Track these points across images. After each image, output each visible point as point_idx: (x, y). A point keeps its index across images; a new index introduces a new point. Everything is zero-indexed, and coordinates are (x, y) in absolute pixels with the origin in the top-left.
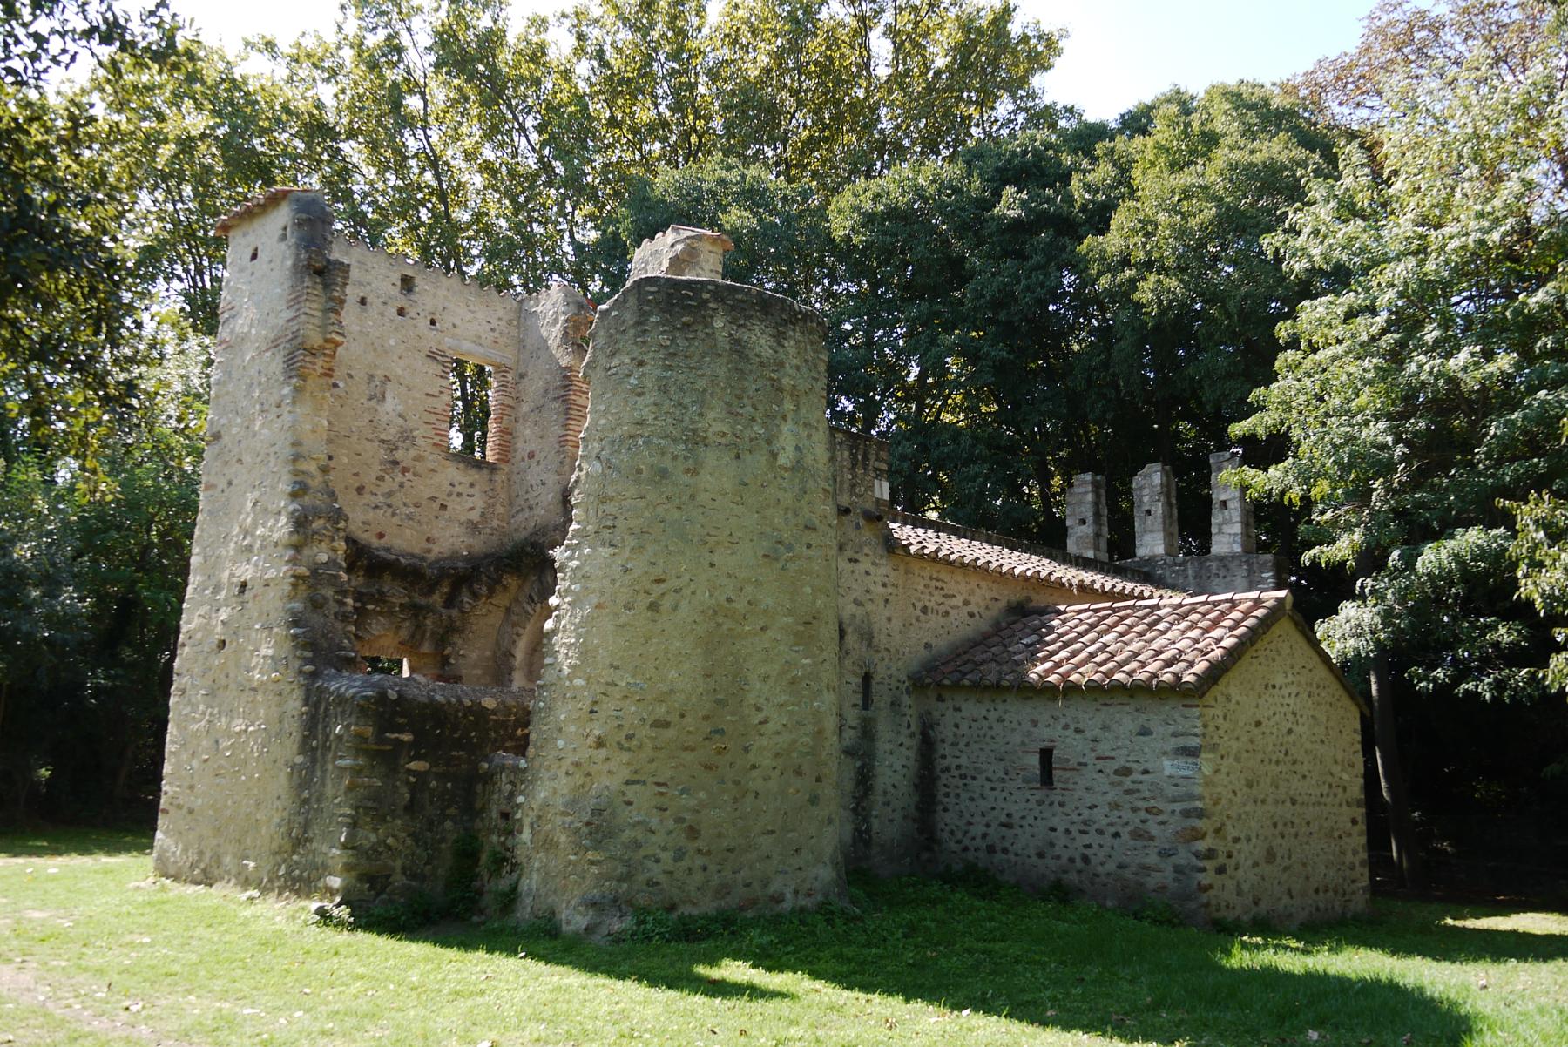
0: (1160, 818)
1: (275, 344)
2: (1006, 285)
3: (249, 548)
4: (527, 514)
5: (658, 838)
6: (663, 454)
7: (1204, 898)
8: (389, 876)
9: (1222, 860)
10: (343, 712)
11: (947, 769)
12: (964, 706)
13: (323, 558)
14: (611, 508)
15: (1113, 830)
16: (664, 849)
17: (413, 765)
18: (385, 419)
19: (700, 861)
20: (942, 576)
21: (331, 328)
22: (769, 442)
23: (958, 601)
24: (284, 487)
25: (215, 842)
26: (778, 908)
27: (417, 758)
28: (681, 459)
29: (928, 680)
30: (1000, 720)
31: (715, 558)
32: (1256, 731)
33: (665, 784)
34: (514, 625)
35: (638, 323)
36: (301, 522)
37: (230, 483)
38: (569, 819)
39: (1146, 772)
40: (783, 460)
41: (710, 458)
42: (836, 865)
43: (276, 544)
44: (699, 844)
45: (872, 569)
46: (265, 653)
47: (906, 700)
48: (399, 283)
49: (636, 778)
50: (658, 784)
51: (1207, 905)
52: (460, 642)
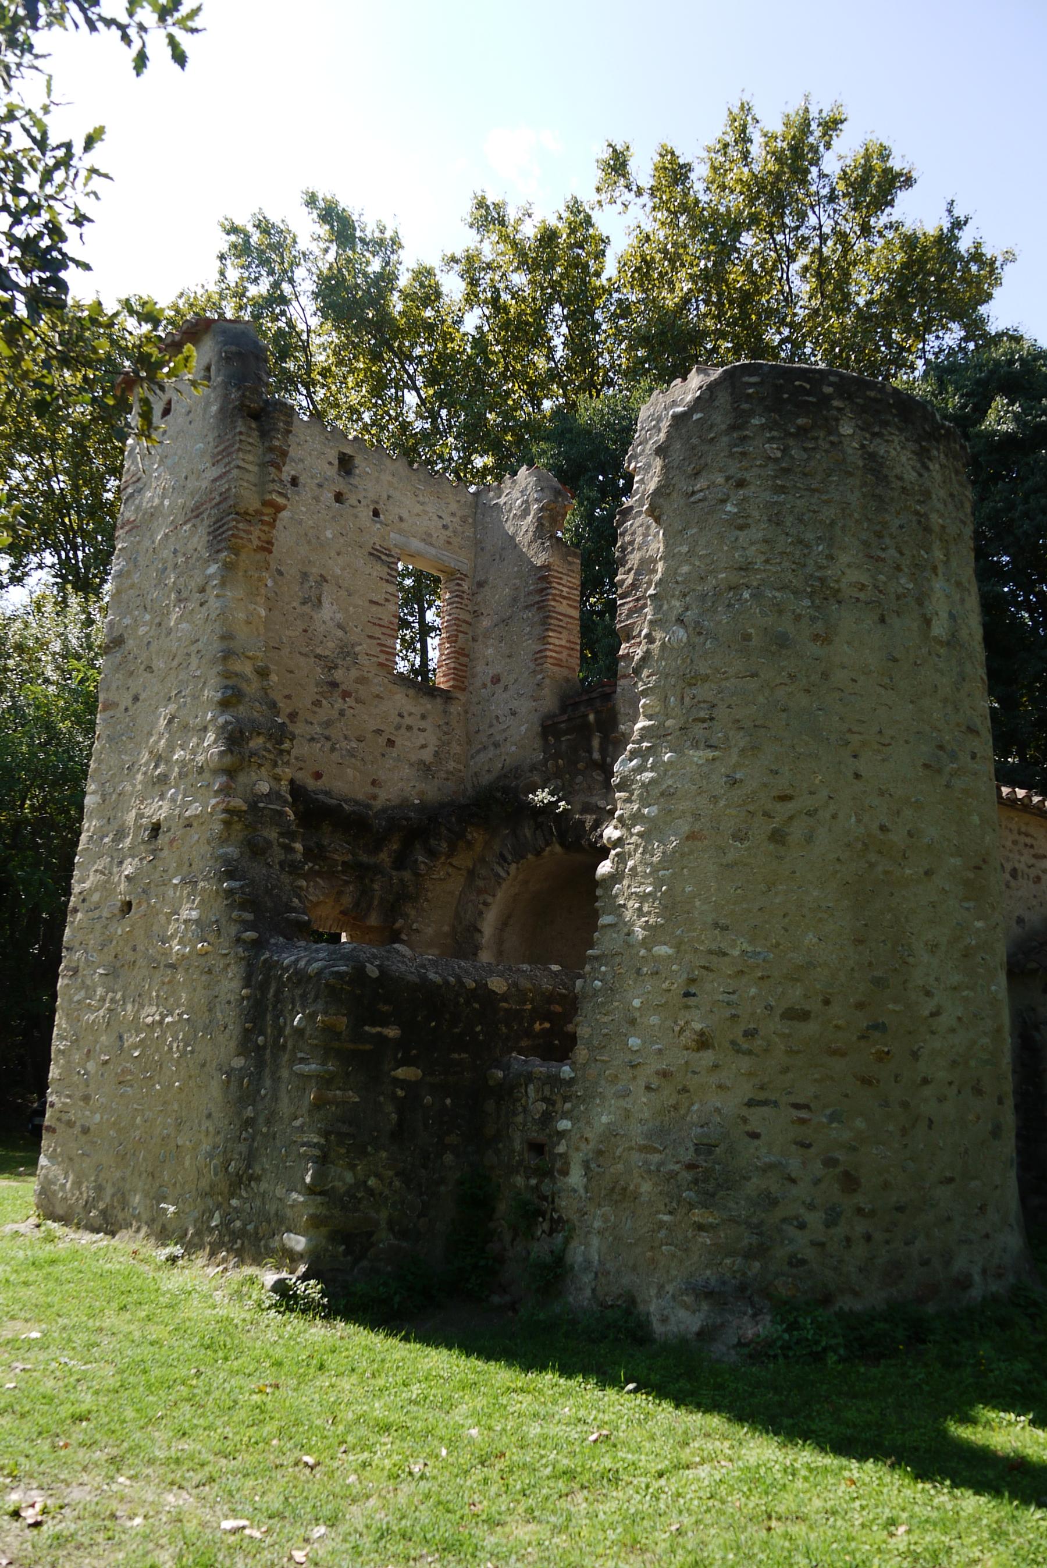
1: (196, 513)
3: (163, 779)
4: (491, 752)
6: (780, 612)
8: (371, 1234)
10: (304, 996)
13: (264, 787)
14: (705, 691)
16: (811, 1207)
17: (401, 1073)
18: (322, 629)
19: (861, 1227)
20: (1032, 830)
21: (271, 486)
22: (920, 603)
24: (211, 693)
25: (118, 1174)
29: (1032, 965)
33: (806, 1107)
34: (480, 892)
35: (733, 428)
36: (234, 739)
37: (136, 699)
38: (656, 1158)
40: (939, 628)
43: (201, 770)
44: (860, 1199)
46: (185, 916)
48: (336, 462)
49: (762, 1096)
50: (796, 1106)
52: (413, 913)
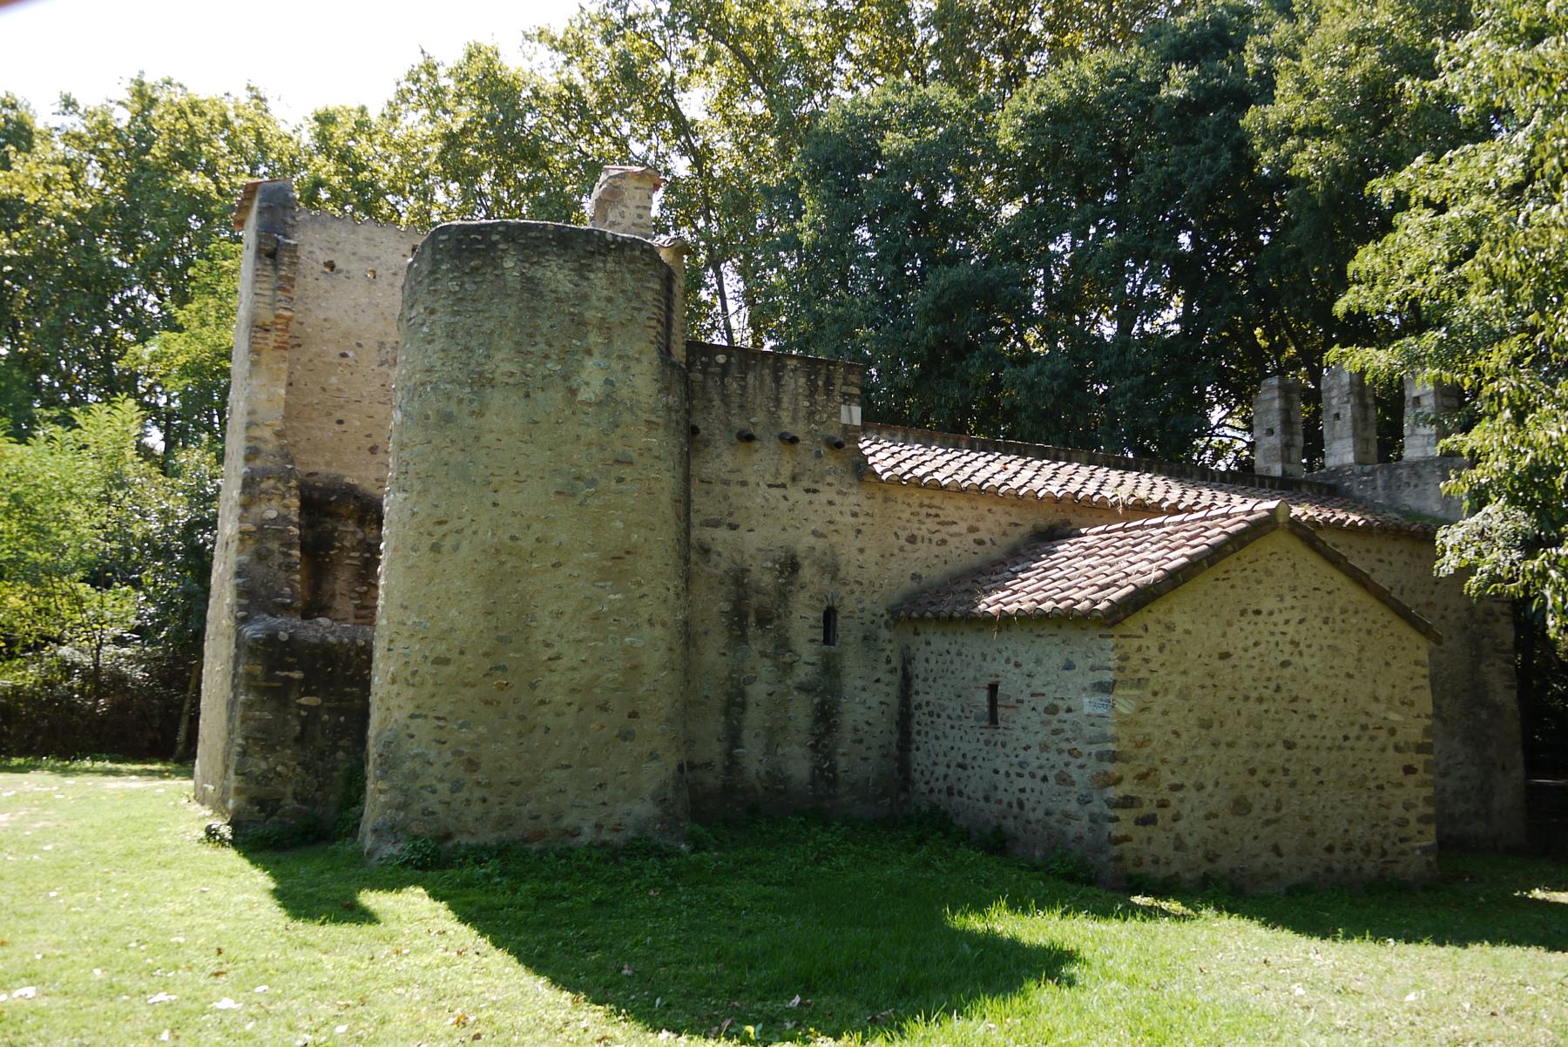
0: (1080, 761)
2: (1170, 175)
5: (435, 770)
7: (1115, 851)
8: (279, 801)
9: (1147, 810)
11: (919, 706)
12: (933, 639)
13: (272, 514)
15: (1041, 773)
16: (441, 780)
17: (304, 701)
19: (478, 793)
22: (566, 378)
23: (962, 527)
26: (572, 842)
27: (308, 693)
28: (466, 402)
30: (959, 654)
31: (500, 498)
32: (1220, 664)
35: (432, 272)
39: (1069, 710)
40: (584, 395)
41: (496, 398)
42: (661, 801)
44: (478, 776)
45: (837, 499)
47: (884, 634)
49: (418, 712)
50: (438, 718)
51: (1119, 858)
